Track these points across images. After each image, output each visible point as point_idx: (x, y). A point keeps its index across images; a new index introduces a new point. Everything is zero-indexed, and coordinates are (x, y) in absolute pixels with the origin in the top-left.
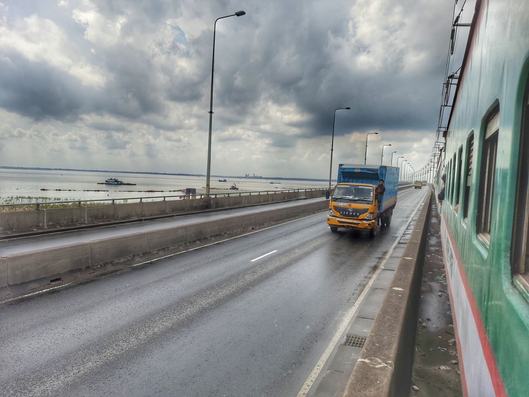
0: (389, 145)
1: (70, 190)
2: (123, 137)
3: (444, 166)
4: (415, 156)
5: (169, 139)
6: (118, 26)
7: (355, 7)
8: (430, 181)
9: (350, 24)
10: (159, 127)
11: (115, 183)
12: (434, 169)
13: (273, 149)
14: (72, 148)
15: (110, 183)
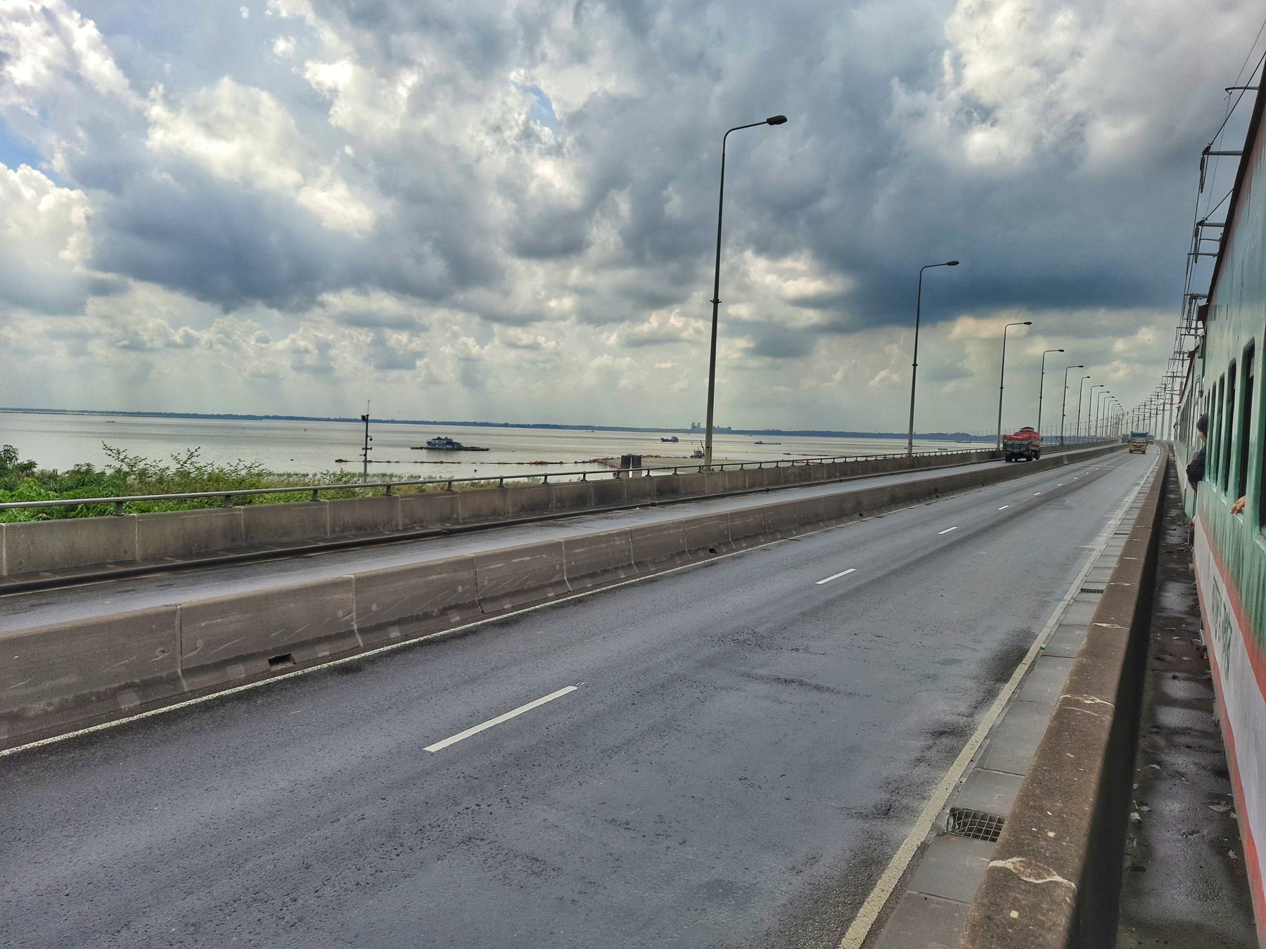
0: (949, 264)
1: (389, 460)
2: (411, 342)
3: (1201, 392)
4: (1121, 373)
5: (512, 345)
6: (403, 92)
7: (957, 19)
8: (1162, 435)
9: (946, 59)
10: (491, 317)
11: (448, 446)
12: (1171, 407)
13: (755, 363)
14: (298, 368)
15: (437, 446)
